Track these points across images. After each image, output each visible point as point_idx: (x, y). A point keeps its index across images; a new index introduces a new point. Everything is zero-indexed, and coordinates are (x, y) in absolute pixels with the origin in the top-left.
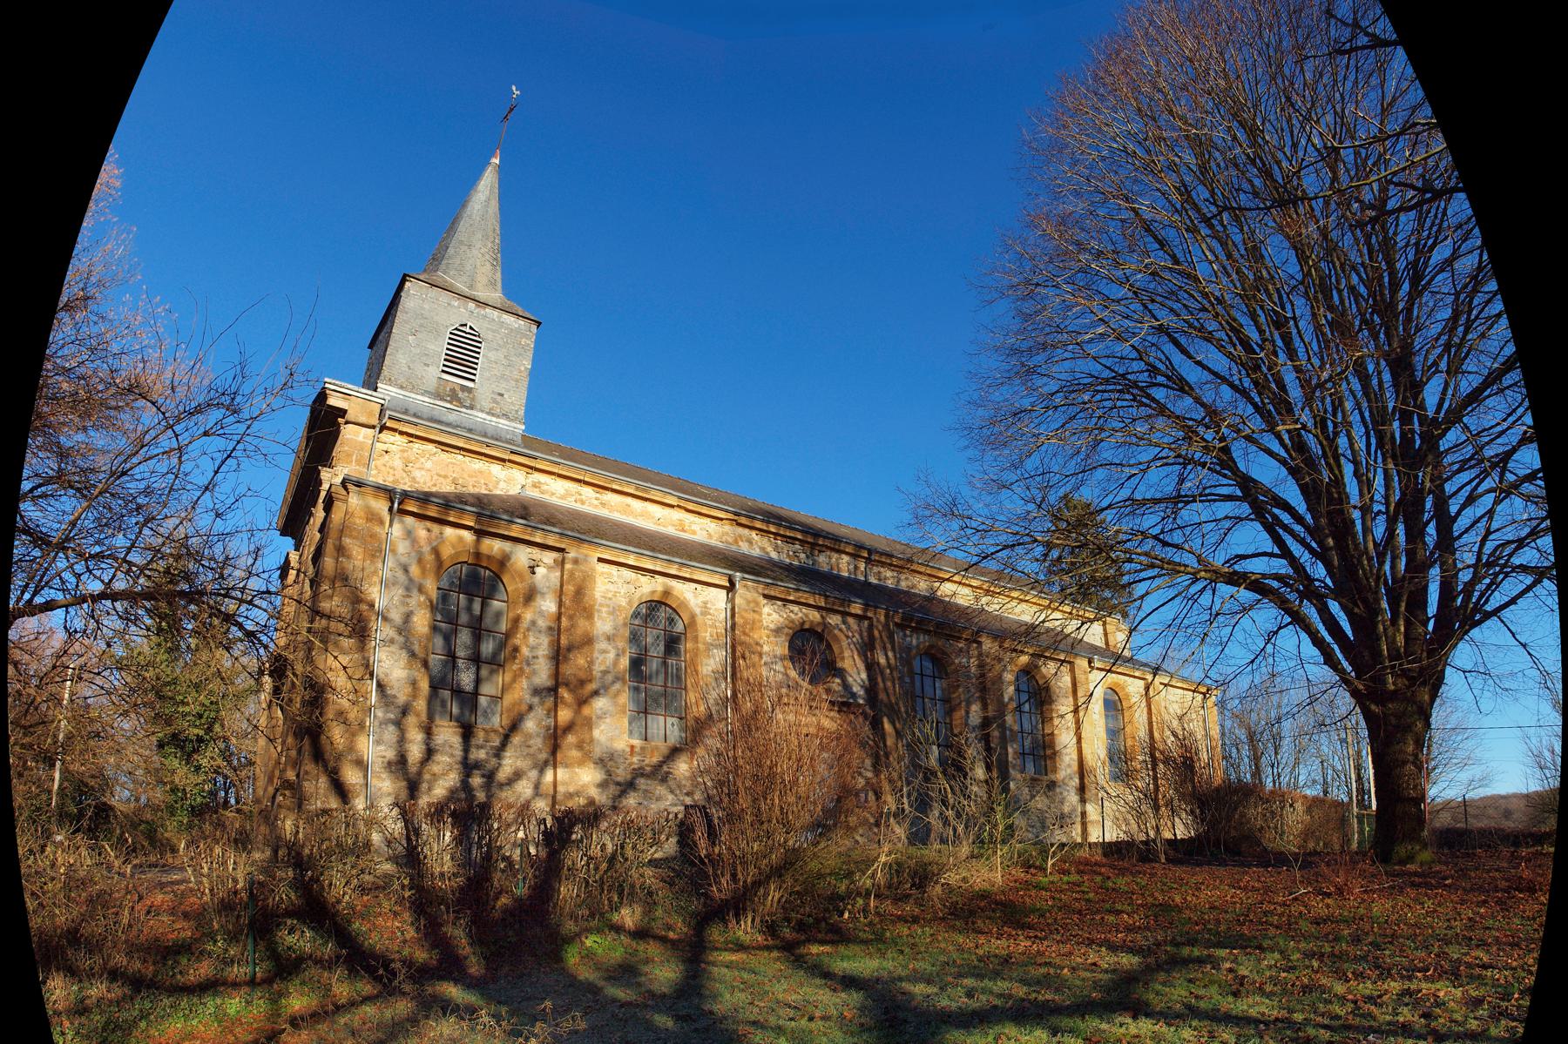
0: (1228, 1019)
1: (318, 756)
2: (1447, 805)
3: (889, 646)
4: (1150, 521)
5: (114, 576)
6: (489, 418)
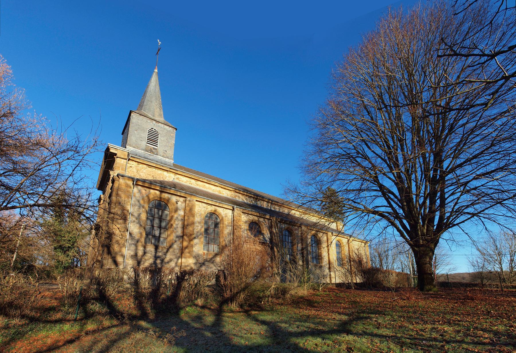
0: (376, 335)
1: (109, 253)
2: (442, 275)
3: (276, 227)
4: (351, 196)
5: (38, 200)
6: (162, 158)
